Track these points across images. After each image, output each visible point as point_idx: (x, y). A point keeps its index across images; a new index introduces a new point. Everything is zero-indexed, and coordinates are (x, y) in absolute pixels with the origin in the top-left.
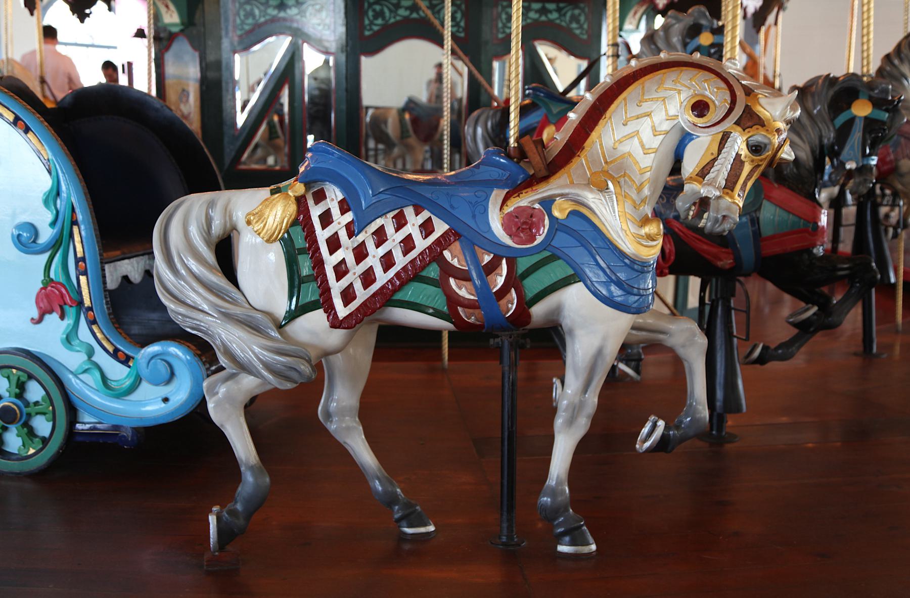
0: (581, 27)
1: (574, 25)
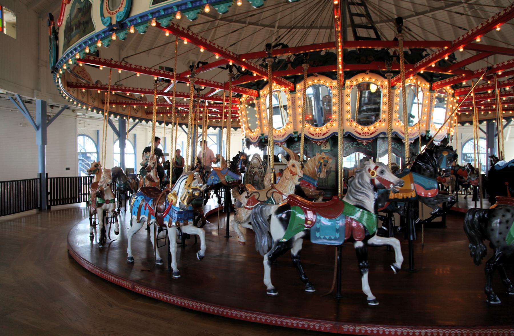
0: (370, 148)
1: (367, 148)
